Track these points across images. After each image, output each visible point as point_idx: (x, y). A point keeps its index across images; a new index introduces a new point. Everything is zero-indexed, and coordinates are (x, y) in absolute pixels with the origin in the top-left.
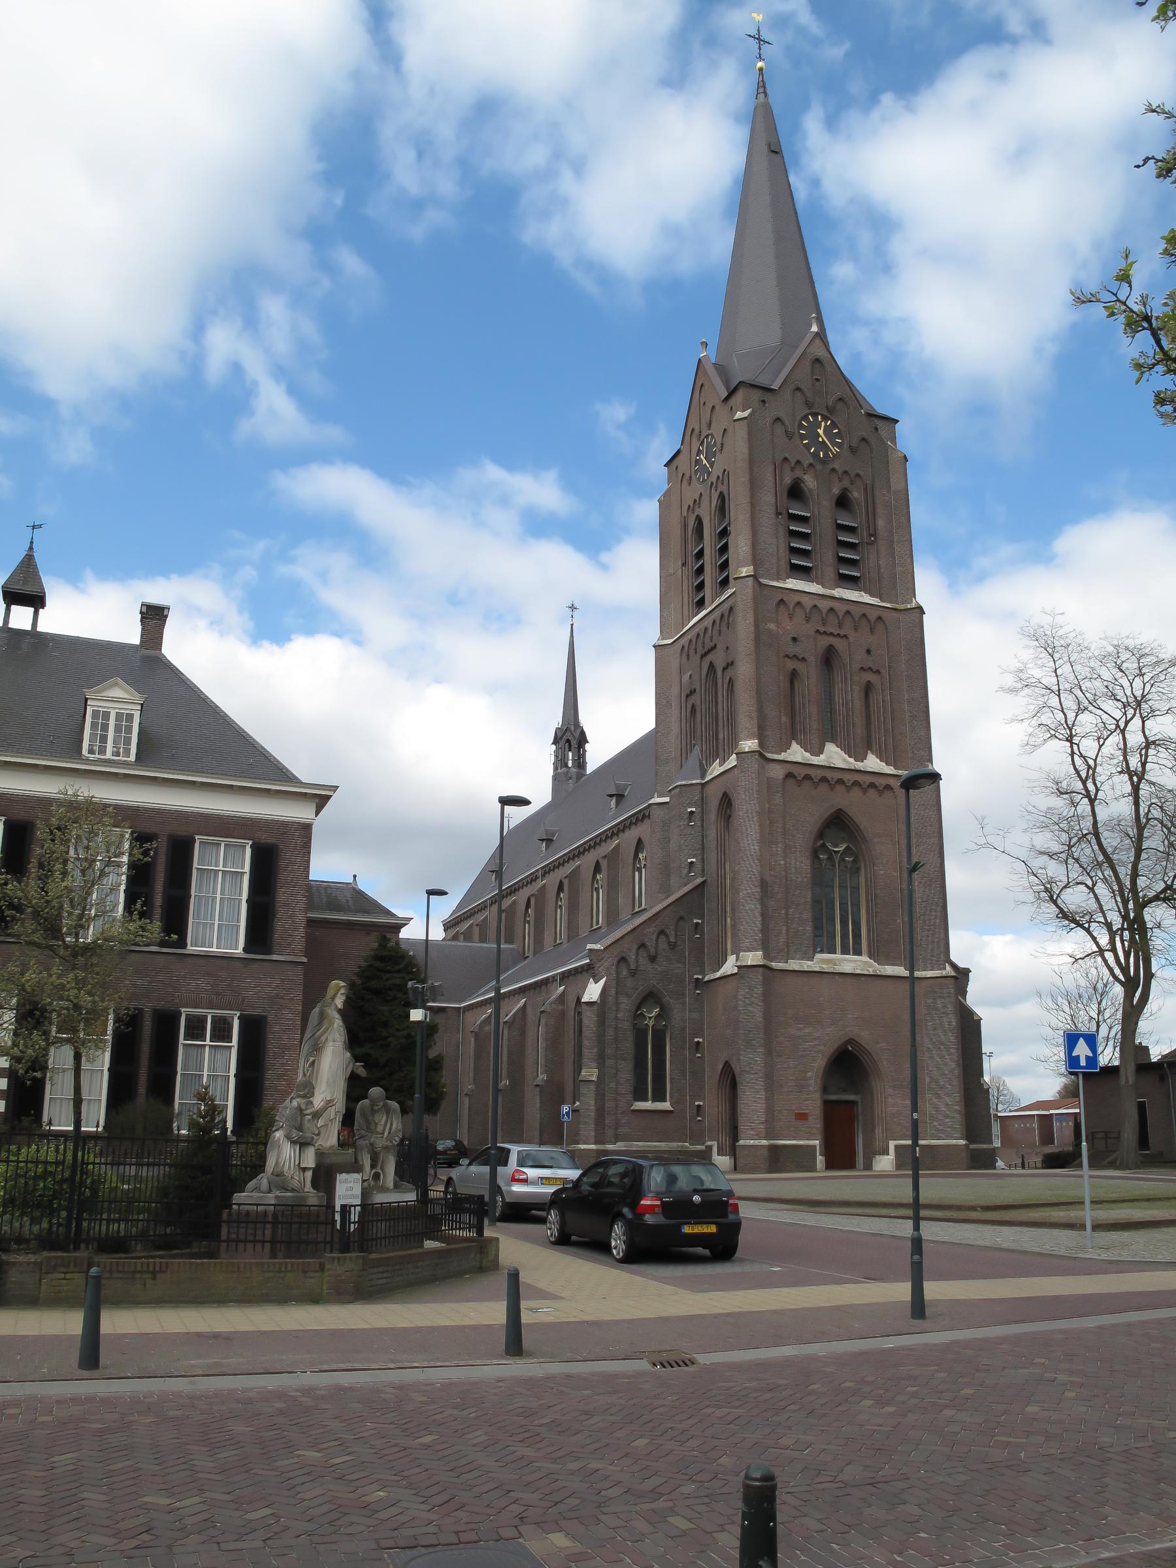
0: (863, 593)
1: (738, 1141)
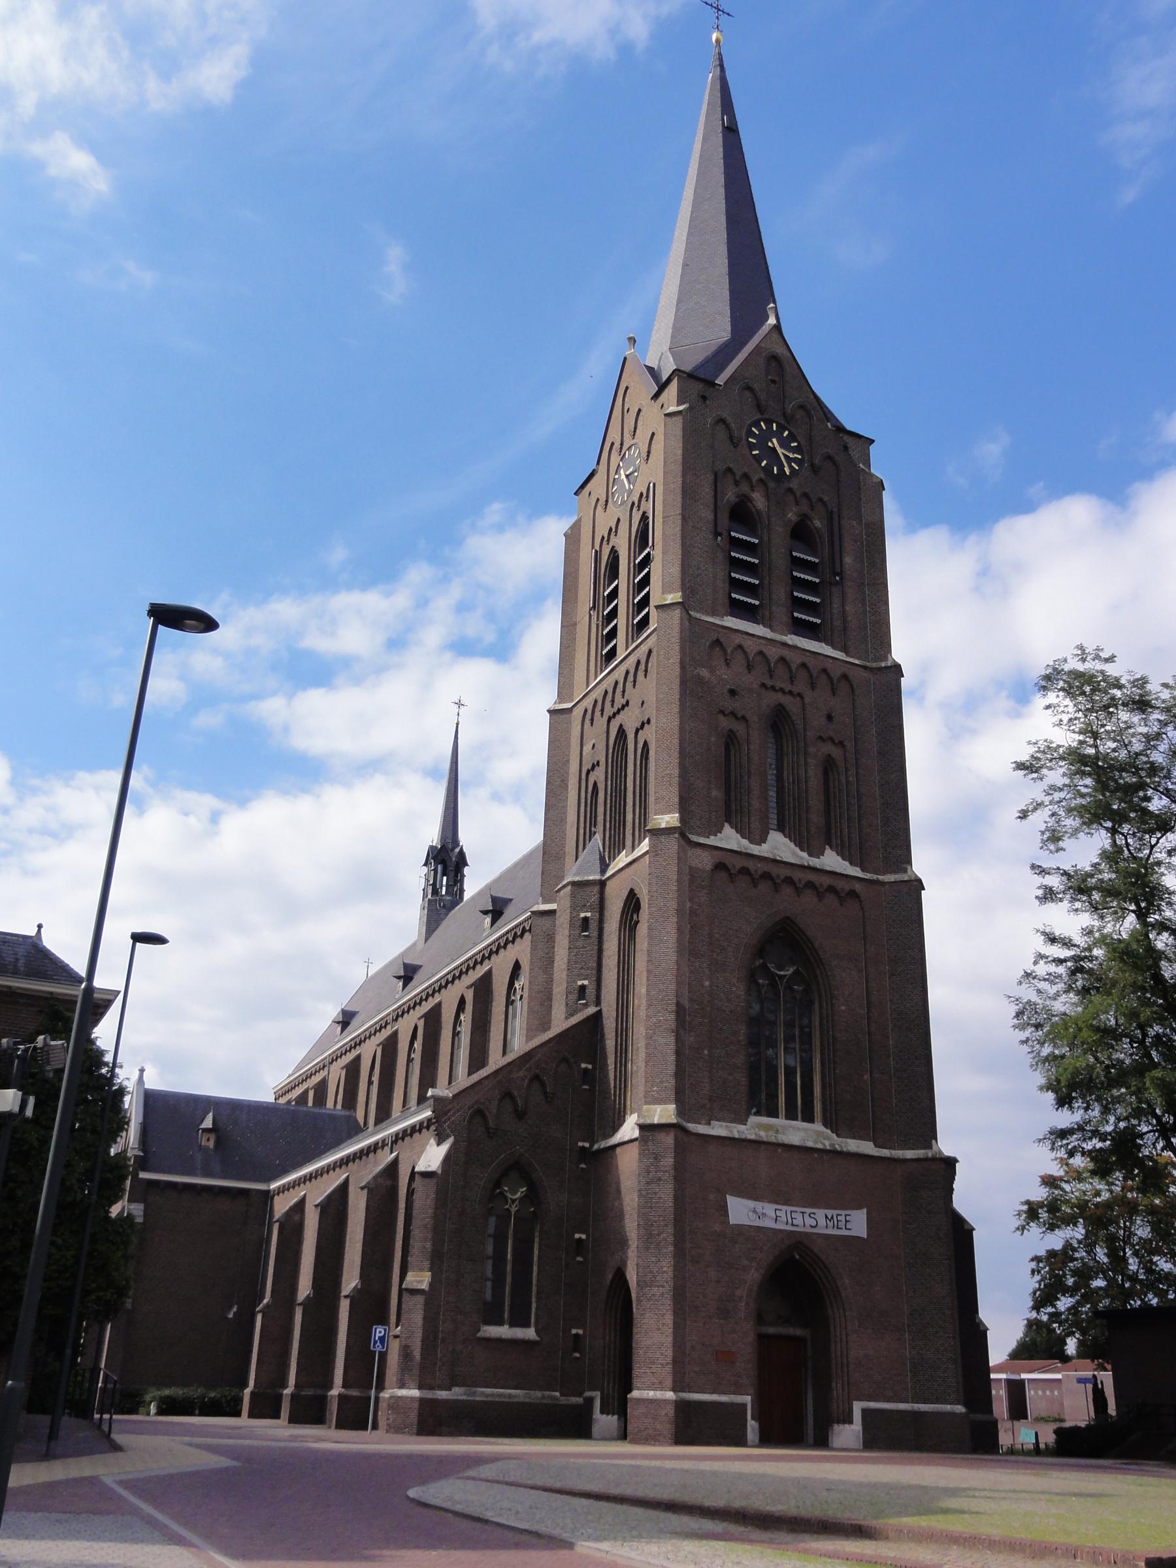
0: (823, 645)
1: (630, 1391)
